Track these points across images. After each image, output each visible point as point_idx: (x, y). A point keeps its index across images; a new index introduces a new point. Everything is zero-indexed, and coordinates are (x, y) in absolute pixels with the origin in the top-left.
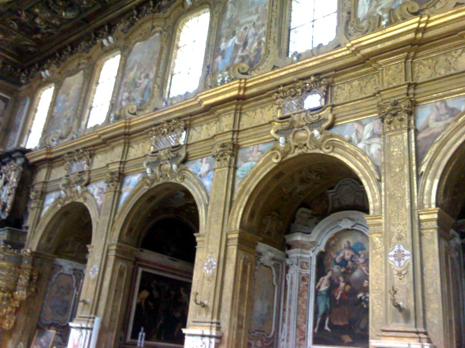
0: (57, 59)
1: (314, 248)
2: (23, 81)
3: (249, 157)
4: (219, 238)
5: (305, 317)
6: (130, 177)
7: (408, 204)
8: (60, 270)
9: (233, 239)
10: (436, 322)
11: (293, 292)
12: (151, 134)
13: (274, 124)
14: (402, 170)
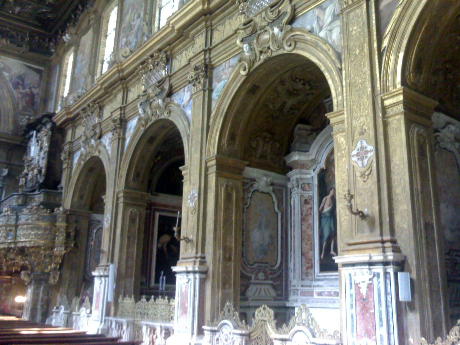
0: (73, 21)
1: (314, 167)
2: (53, 50)
3: (222, 76)
4: (198, 168)
5: (311, 243)
6: (131, 121)
7: (369, 90)
8: (98, 225)
9: (212, 166)
10: (406, 226)
11: (296, 217)
12: (141, 73)
13: (239, 32)
14: (363, 49)
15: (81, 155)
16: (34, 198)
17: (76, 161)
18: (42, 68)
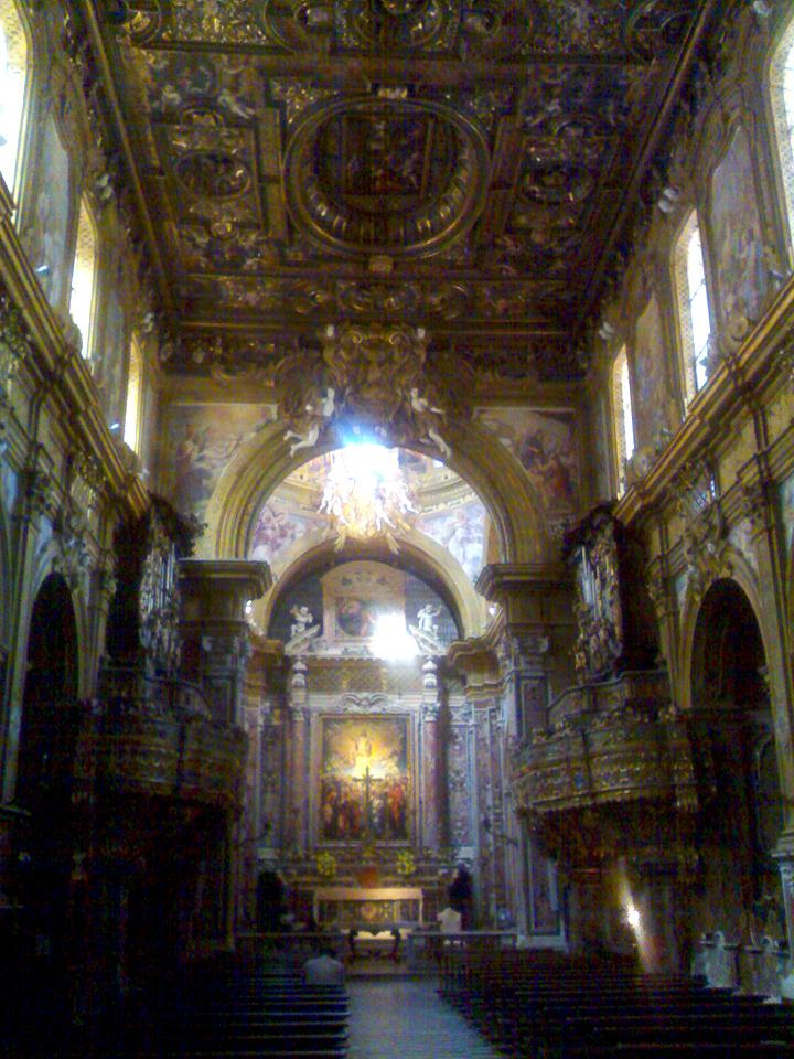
15: (691, 581)
16: (610, 693)
17: (682, 596)
18: (571, 410)
